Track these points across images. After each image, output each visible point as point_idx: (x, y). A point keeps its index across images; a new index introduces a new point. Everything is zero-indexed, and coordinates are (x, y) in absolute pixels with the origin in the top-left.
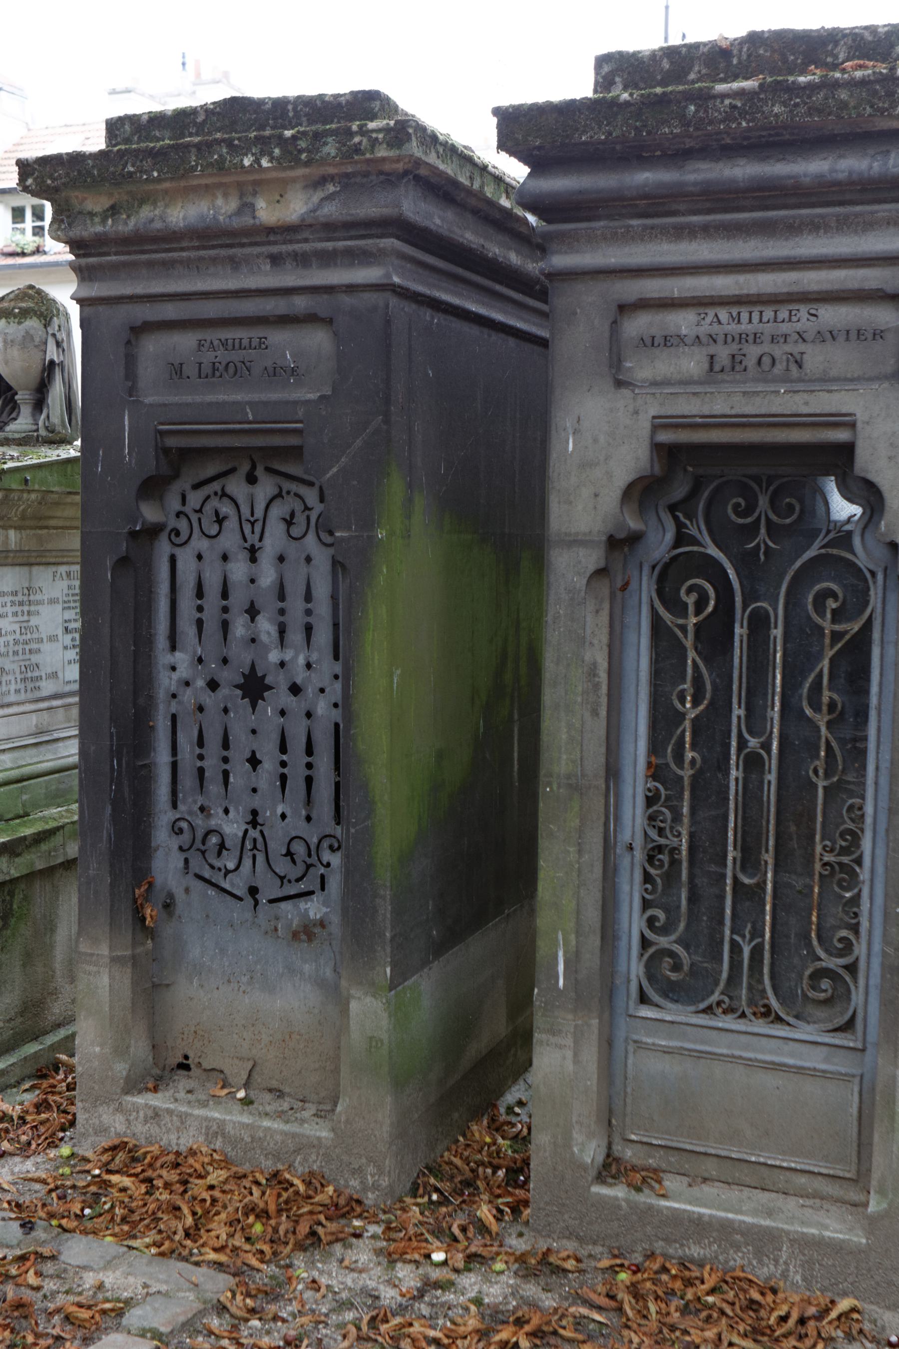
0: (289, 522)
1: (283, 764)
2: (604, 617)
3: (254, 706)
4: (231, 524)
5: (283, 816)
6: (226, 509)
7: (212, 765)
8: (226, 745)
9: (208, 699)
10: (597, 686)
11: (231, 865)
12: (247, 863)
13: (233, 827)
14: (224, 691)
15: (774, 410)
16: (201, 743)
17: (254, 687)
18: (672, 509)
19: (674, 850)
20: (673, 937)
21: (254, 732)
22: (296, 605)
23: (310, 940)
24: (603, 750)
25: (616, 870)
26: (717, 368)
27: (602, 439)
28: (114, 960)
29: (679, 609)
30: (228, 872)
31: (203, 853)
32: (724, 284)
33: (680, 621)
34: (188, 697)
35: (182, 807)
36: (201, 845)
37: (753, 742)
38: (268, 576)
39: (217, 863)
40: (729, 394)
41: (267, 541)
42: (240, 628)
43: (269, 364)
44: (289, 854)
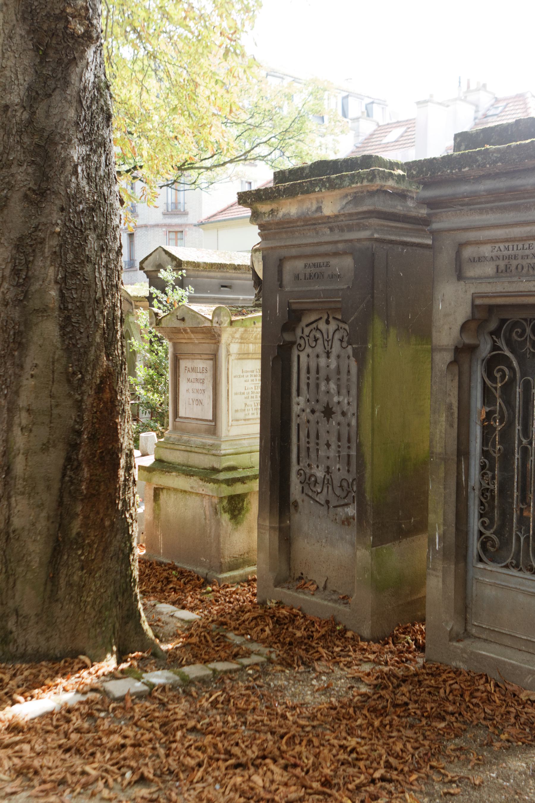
0: (341, 341)
1: (339, 446)
2: (456, 383)
3: (328, 421)
4: (320, 342)
5: (339, 469)
6: (318, 335)
7: (312, 445)
8: (318, 437)
9: (311, 417)
10: (452, 414)
11: (319, 491)
12: (325, 490)
13: (320, 473)
14: (317, 414)
15: (522, 289)
16: (308, 436)
17: (328, 412)
18: (491, 333)
19: (492, 491)
20: (492, 531)
21: (328, 432)
22: (344, 376)
23: (349, 525)
24: (456, 443)
25: (467, 499)
26: (500, 271)
27: (453, 303)
28: (271, 528)
29: (493, 379)
30: (318, 493)
31: (309, 484)
32: (500, 233)
33: (494, 385)
34: (304, 416)
35: (301, 464)
36: (308, 481)
37: (525, 441)
38: (333, 366)
39: (314, 489)
40: (503, 282)
41: (333, 349)
42: (323, 388)
43: (330, 273)
44: (341, 486)
